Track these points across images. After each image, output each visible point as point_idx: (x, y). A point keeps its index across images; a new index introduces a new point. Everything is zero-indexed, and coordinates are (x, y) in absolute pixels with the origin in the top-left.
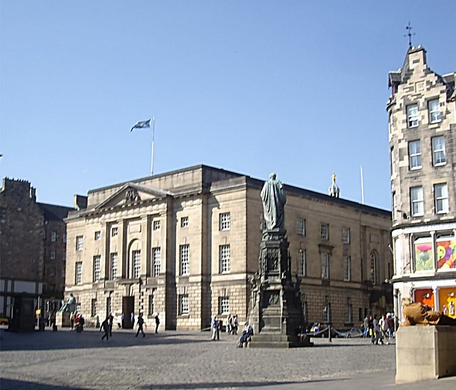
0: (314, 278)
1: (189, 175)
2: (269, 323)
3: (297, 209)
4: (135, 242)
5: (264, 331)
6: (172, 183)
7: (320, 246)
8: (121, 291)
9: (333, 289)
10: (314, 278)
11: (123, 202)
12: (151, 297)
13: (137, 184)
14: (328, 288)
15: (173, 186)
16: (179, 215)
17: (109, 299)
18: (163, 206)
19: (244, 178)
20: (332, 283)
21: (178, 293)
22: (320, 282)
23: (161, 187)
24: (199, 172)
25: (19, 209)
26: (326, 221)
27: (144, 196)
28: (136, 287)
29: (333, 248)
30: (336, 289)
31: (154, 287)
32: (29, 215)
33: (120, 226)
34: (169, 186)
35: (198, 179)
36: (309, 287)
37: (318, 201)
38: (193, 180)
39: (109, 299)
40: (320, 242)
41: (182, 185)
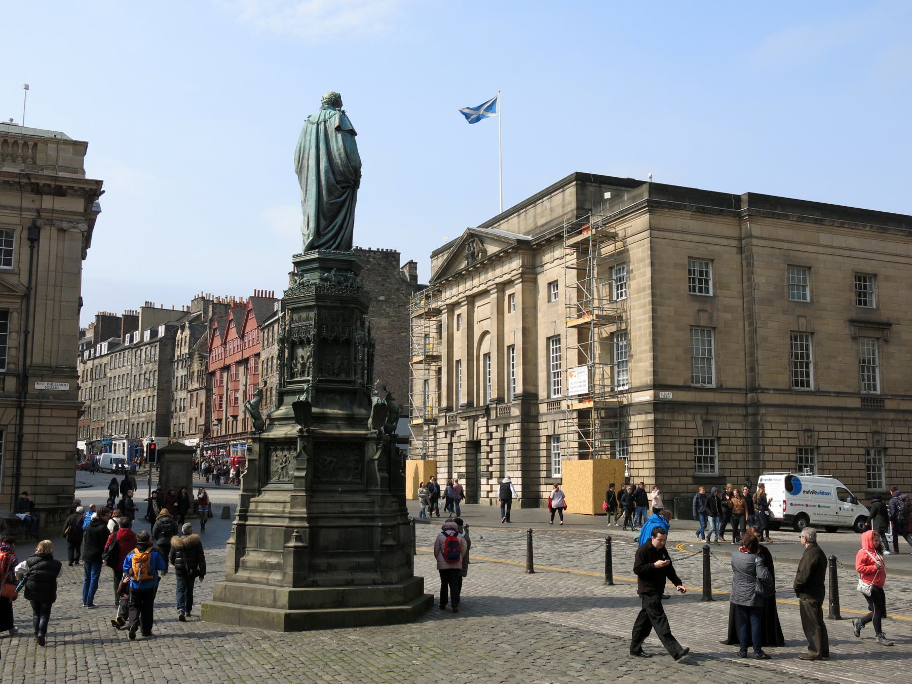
0: (838, 394)
1: (558, 198)
2: (261, 544)
3: (785, 245)
4: (488, 337)
5: (246, 568)
6: (535, 217)
7: (852, 322)
8: (463, 432)
9: (892, 416)
10: (838, 394)
11: (464, 265)
12: (503, 440)
13: (489, 230)
14: (878, 415)
15: (536, 223)
16: (542, 281)
17: (451, 444)
18: (515, 265)
19: (645, 188)
20: (889, 404)
21: (543, 433)
22: (856, 403)
23: (514, 229)
24: (571, 191)
25: (382, 298)
26: (867, 267)
27: (492, 249)
28: (482, 422)
29: (891, 325)
30: (900, 417)
31: (505, 422)
32: (399, 306)
33: (463, 310)
34: (531, 226)
35: (570, 203)
36: (825, 413)
37: (865, 226)
38: (563, 207)
39: (451, 444)
40: (853, 315)
41: (548, 219)
